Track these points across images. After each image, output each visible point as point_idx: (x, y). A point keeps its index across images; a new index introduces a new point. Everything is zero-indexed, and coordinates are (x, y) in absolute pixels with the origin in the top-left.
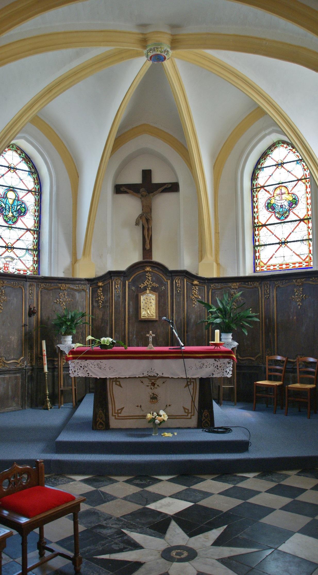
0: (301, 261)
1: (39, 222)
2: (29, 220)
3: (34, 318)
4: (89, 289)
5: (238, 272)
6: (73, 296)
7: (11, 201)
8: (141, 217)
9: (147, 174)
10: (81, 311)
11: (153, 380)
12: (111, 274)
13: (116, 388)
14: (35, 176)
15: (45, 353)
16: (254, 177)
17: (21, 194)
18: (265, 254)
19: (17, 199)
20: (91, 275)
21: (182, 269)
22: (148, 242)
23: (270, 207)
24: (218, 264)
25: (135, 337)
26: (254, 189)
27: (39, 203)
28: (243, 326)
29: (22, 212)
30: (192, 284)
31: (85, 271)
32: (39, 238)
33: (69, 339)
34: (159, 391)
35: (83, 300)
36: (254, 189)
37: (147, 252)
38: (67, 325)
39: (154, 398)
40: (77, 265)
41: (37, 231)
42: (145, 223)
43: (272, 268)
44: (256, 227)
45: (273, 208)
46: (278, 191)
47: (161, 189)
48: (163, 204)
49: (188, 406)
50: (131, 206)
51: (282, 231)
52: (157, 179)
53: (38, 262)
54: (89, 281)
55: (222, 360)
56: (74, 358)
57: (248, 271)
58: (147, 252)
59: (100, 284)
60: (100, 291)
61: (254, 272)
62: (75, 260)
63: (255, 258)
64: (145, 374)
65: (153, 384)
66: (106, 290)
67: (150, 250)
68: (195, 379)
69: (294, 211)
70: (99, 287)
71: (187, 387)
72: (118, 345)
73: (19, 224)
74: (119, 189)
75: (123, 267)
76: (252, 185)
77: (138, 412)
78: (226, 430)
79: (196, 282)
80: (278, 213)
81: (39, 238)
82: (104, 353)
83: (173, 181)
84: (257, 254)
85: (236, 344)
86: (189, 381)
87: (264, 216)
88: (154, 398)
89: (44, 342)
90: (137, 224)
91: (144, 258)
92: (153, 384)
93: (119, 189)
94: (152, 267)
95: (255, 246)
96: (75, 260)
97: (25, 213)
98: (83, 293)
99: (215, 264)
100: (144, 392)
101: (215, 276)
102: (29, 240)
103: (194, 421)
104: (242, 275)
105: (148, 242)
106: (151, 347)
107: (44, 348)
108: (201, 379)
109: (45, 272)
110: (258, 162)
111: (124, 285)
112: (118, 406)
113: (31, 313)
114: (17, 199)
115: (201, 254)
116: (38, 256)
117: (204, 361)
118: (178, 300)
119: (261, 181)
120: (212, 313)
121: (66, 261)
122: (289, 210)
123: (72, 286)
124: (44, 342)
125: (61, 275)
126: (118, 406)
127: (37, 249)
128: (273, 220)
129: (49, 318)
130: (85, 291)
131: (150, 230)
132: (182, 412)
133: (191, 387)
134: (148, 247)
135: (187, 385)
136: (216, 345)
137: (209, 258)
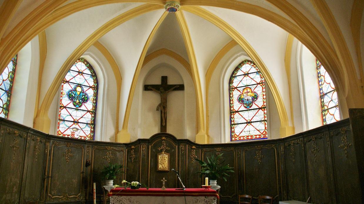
2: (89, 105)
3: (89, 168)
4: (125, 150)
5: (221, 141)
6: (115, 155)
7: (78, 93)
8: (160, 105)
9: (164, 79)
14: (95, 78)
16: (231, 82)
19: (83, 92)
21: (185, 138)
22: (164, 121)
23: (241, 100)
24: (208, 136)
27: (96, 95)
28: (224, 176)
29: (85, 100)
31: (124, 139)
32: (95, 117)
33: (111, 182)
35: (122, 157)
36: (231, 89)
37: (163, 127)
40: (119, 135)
41: (94, 112)
42: (163, 110)
44: (232, 112)
45: (243, 101)
46: (245, 91)
48: (174, 97)
50: (154, 98)
51: (248, 115)
52: (171, 81)
53: (93, 132)
54: (126, 145)
56: (113, 195)
57: (227, 140)
58: (163, 127)
59: (133, 147)
62: (117, 131)
66: (137, 151)
70: (132, 149)
73: (83, 108)
74: (147, 88)
75: (148, 137)
79: (194, 147)
80: (246, 104)
83: (181, 83)
85: (219, 187)
89: (95, 184)
90: (157, 110)
93: (147, 88)
95: (231, 125)
97: (87, 101)
98: (122, 153)
99: (206, 136)
101: (206, 143)
104: (223, 142)
105: (164, 121)
107: (95, 188)
110: (233, 73)
114: (83, 92)
116: (94, 128)
117: (198, 198)
119: (235, 84)
120: (204, 167)
125: (108, 141)
127: (93, 124)
128: (243, 108)
131: (165, 113)
134: (164, 124)
136: (206, 187)
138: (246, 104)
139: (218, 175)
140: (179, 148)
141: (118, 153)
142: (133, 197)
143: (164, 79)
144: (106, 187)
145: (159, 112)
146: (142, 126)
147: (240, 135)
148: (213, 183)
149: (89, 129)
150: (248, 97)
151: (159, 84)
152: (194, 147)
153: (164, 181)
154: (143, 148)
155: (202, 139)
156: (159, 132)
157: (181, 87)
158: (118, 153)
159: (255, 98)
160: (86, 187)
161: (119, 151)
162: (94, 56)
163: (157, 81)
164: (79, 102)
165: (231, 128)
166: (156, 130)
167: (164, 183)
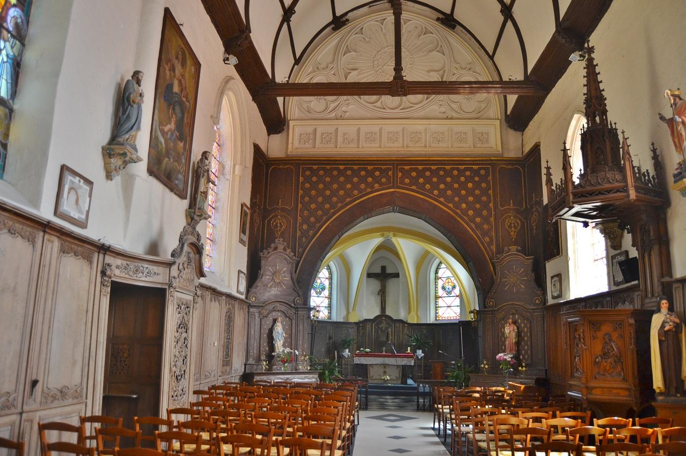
0: (456, 316)
1: (331, 294)
2: (326, 293)
3: (331, 340)
4: (356, 328)
5: (427, 321)
6: (348, 331)
7: (319, 284)
8: (380, 290)
9: (383, 268)
10: (351, 338)
11: (385, 366)
12: (366, 321)
13: (371, 368)
14: (329, 271)
15: (336, 357)
16: (437, 272)
17: (323, 280)
18: (441, 311)
19: (321, 283)
20: (356, 320)
21: (400, 318)
22: (384, 303)
23: (443, 288)
24: (418, 316)
25: (378, 348)
26: (437, 278)
27: (331, 284)
28: (426, 347)
29: (323, 289)
30: (404, 326)
31: (354, 319)
32: (331, 301)
33: (347, 350)
34: (387, 370)
35: (352, 333)
36: (437, 278)
37: (383, 309)
38: (345, 344)
39: (385, 372)
40: (349, 315)
41: (330, 297)
42: (382, 293)
43: (444, 318)
44: (437, 297)
45: (445, 289)
46: (447, 281)
47: (392, 276)
48: (391, 284)
49: (398, 376)
50: (376, 285)
51: (449, 300)
52: (389, 270)
53: (330, 313)
54: (355, 323)
55: (410, 359)
56: (356, 356)
57: (432, 320)
58: (383, 309)
59: (361, 325)
60: (360, 328)
61: (436, 320)
62: (348, 313)
63: (436, 313)
64: (382, 363)
65: (385, 367)
66: (364, 328)
67: (385, 308)
68: (400, 365)
69: (454, 291)
70: (360, 326)
71: (338, 14)
72: (372, 352)
73: (322, 295)
74: (369, 275)
75: (372, 318)
76: (436, 276)
77: (379, 377)
78: (409, 385)
79: (406, 325)
80: (447, 292)
81: (331, 301)
82: (367, 355)
83: (397, 272)
84: (437, 311)
85: (423, 355)
86: (398, 366)
87: (441, 292)
88: (385, 372)
89: (336, 352)
90: (378, 294)
91: (381, 313)
92: (385, 367)
93: (369, 275)
94: (385, 318)
95: (436, 307)
96: (348, 313)
97: (325, 289)
98: (353, 329)
99: (416, 317)
100: (382, 370)
101: (415, 322)
102: (326, 302)
103: (400, 381)
104: (428, 322)
105: (384, 303)
106: (384, 353)
107: (336, 354)
108: (403, 366)
109: (334, 318)
110: (439, 265)
111: (372, 325)
112: (371, 375)
113: (330, 338)
114: (321, 283)
115: (409, 311)
116: (330, 310)
117: (404, 359)
118: (181, 145)
119: (440, 275)
120: (412, 340)
121: (344, 313)
122: (452, 291)
123: (348, 326)
124: (336, 352)
125: (342, 321)
126: (371, 375)
127: (330, 307)
128: (445, 295)
129: (63, 400)
130: (353, 328)
131: (385, 297)
132: (395, 378)
133: (399, 369)
134: (384, 306)
135: (397, 368)
136: (408, 353)
137: (413, 313)
138: (447, 292)
139: (422, 347)
140: (395, 326)
141: (350, 330)
142: (367, 358)
143: (383, 268)
144: (344, 354)
145: (380, 296)
146: (369, 310)
147: (442, 316)
148: (633, 343)
149: (327, 311)
150: (449, 286)
151: (378, 272)
152: (406, 325)
153: (384, 349)
154: (368, 326)
155: (413, 319)
156: (380, 314)
157: (397, 275)
158: (350, 330)
159: (454, 287)
160: (329, 354)
161: (351, 328)
162: (336, 264)
163: (378, 270)
164: (320, 291)
165: (436, 310)
166: (377, 312)
167: (464, 429)
